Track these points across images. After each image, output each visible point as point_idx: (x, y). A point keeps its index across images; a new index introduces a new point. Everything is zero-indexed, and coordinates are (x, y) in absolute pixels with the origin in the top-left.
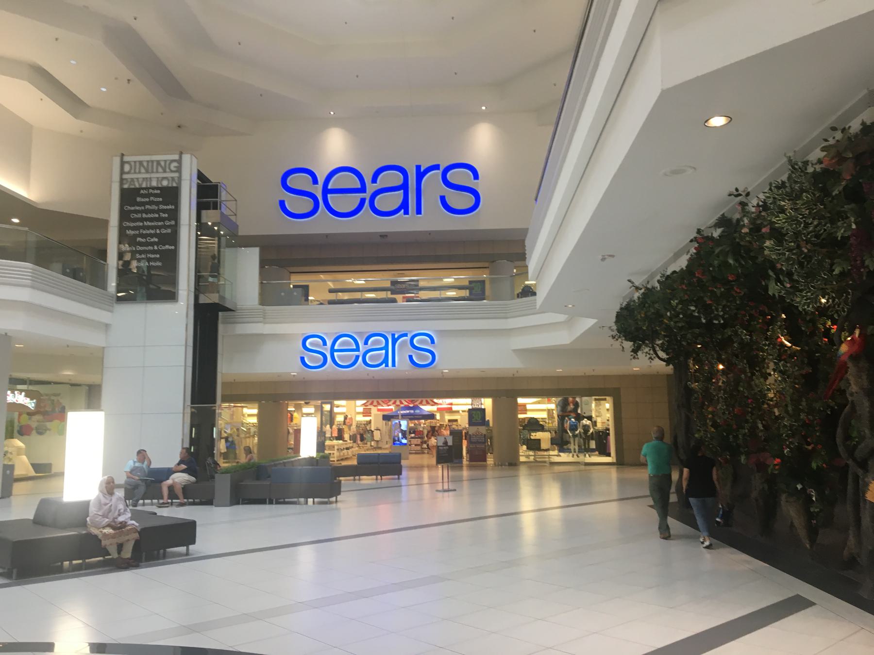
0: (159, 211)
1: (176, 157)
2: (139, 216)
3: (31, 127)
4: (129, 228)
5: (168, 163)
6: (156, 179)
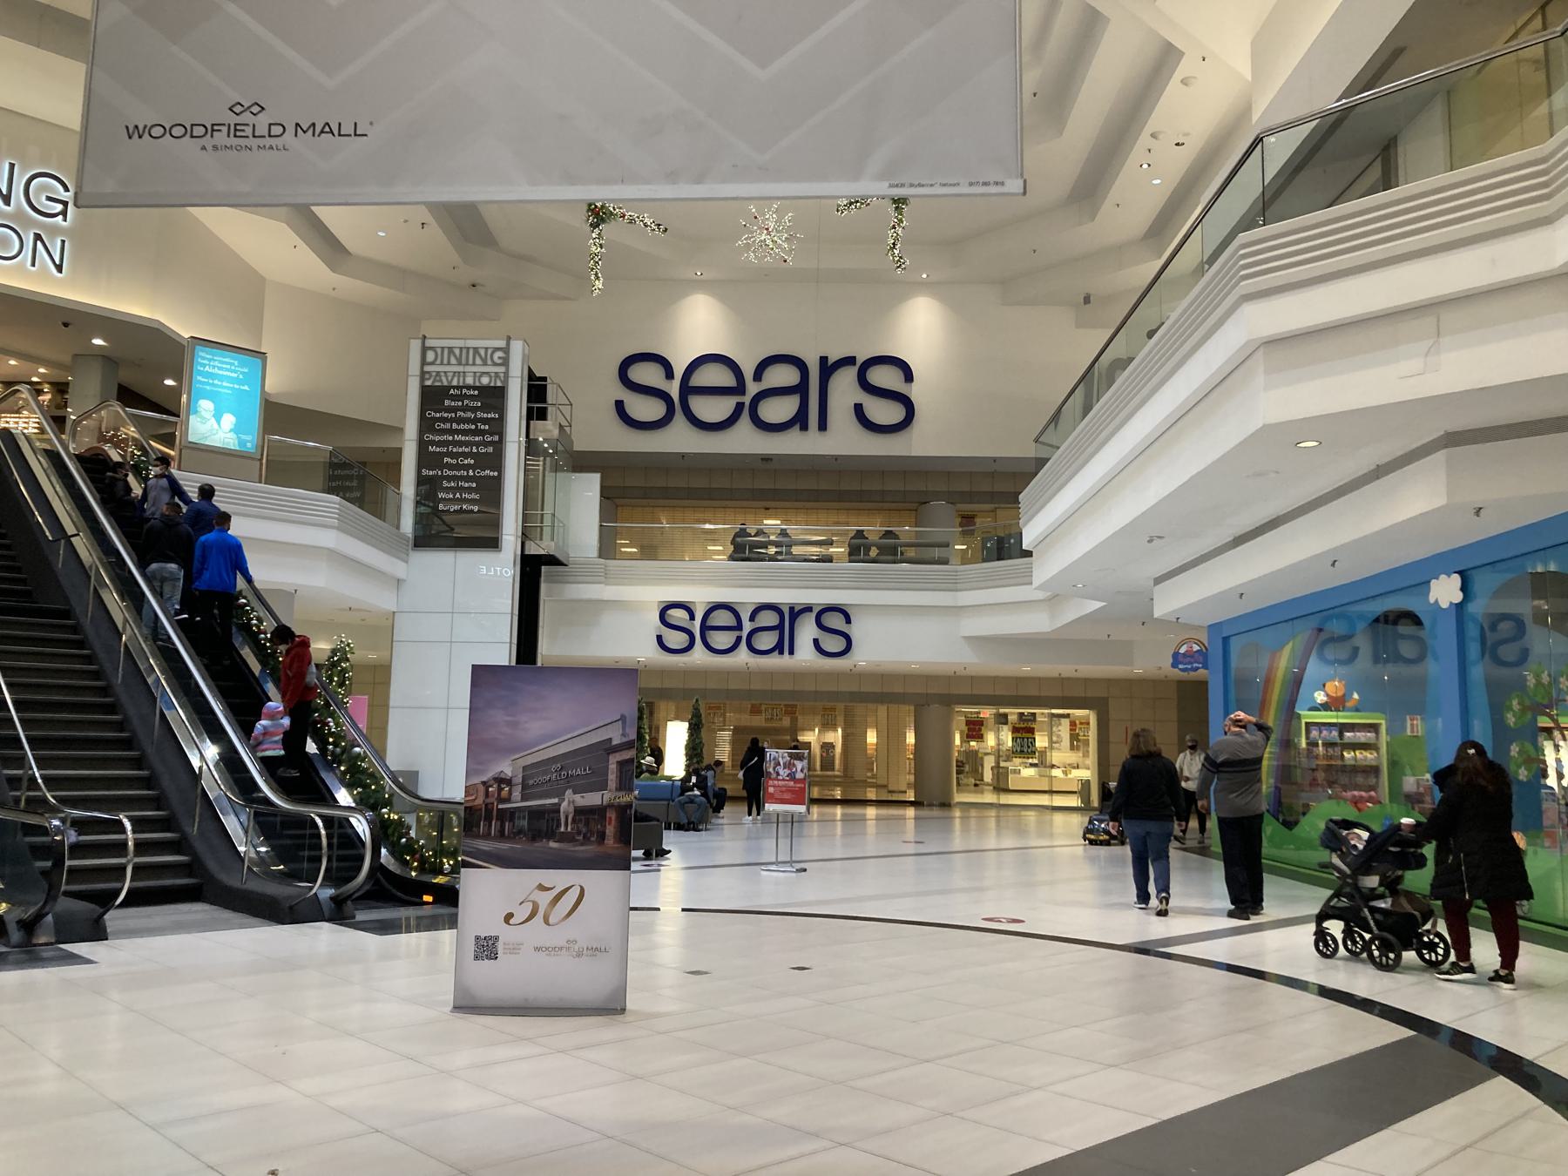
0: (475, 421)
1: (502, 344)
2: (448, 426)
3: (263, 279)
4: (433, 443)
5: (490, 352)
6: (472, 374)
